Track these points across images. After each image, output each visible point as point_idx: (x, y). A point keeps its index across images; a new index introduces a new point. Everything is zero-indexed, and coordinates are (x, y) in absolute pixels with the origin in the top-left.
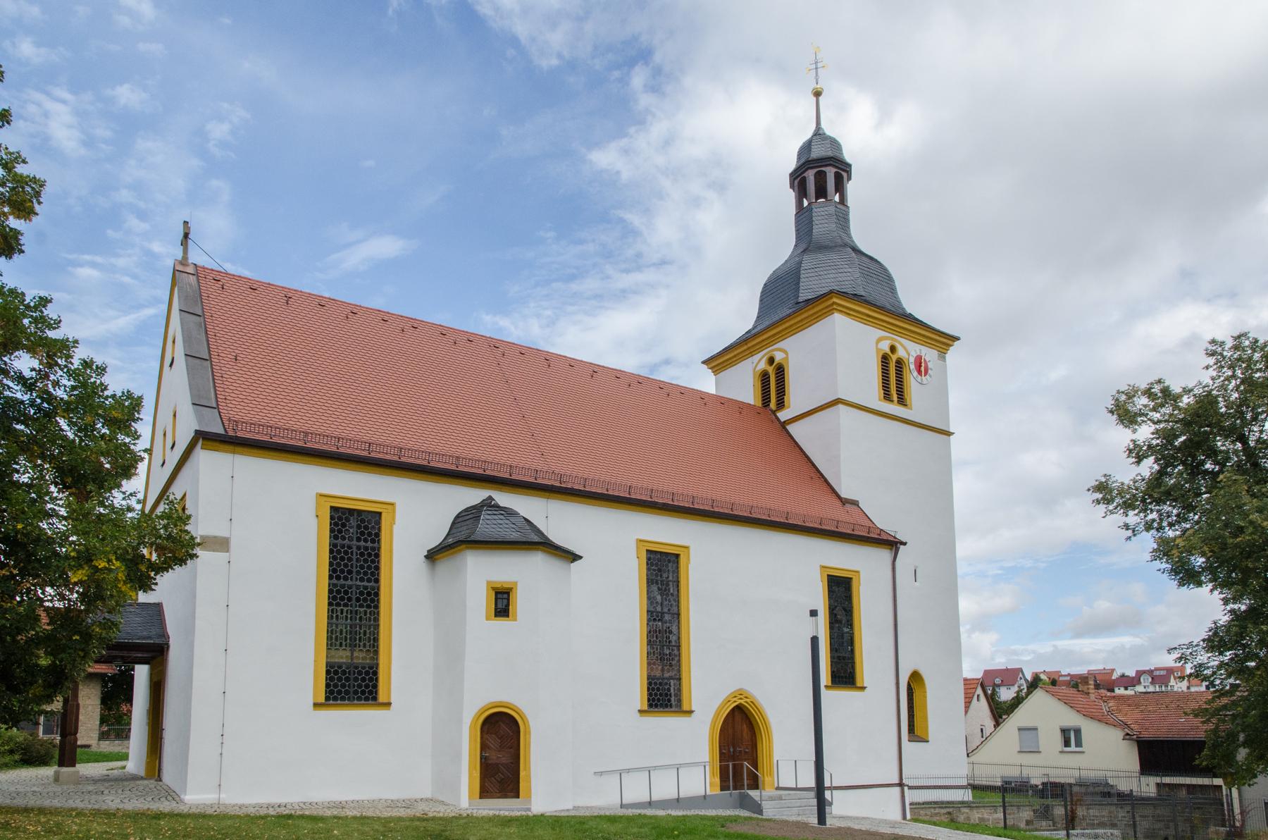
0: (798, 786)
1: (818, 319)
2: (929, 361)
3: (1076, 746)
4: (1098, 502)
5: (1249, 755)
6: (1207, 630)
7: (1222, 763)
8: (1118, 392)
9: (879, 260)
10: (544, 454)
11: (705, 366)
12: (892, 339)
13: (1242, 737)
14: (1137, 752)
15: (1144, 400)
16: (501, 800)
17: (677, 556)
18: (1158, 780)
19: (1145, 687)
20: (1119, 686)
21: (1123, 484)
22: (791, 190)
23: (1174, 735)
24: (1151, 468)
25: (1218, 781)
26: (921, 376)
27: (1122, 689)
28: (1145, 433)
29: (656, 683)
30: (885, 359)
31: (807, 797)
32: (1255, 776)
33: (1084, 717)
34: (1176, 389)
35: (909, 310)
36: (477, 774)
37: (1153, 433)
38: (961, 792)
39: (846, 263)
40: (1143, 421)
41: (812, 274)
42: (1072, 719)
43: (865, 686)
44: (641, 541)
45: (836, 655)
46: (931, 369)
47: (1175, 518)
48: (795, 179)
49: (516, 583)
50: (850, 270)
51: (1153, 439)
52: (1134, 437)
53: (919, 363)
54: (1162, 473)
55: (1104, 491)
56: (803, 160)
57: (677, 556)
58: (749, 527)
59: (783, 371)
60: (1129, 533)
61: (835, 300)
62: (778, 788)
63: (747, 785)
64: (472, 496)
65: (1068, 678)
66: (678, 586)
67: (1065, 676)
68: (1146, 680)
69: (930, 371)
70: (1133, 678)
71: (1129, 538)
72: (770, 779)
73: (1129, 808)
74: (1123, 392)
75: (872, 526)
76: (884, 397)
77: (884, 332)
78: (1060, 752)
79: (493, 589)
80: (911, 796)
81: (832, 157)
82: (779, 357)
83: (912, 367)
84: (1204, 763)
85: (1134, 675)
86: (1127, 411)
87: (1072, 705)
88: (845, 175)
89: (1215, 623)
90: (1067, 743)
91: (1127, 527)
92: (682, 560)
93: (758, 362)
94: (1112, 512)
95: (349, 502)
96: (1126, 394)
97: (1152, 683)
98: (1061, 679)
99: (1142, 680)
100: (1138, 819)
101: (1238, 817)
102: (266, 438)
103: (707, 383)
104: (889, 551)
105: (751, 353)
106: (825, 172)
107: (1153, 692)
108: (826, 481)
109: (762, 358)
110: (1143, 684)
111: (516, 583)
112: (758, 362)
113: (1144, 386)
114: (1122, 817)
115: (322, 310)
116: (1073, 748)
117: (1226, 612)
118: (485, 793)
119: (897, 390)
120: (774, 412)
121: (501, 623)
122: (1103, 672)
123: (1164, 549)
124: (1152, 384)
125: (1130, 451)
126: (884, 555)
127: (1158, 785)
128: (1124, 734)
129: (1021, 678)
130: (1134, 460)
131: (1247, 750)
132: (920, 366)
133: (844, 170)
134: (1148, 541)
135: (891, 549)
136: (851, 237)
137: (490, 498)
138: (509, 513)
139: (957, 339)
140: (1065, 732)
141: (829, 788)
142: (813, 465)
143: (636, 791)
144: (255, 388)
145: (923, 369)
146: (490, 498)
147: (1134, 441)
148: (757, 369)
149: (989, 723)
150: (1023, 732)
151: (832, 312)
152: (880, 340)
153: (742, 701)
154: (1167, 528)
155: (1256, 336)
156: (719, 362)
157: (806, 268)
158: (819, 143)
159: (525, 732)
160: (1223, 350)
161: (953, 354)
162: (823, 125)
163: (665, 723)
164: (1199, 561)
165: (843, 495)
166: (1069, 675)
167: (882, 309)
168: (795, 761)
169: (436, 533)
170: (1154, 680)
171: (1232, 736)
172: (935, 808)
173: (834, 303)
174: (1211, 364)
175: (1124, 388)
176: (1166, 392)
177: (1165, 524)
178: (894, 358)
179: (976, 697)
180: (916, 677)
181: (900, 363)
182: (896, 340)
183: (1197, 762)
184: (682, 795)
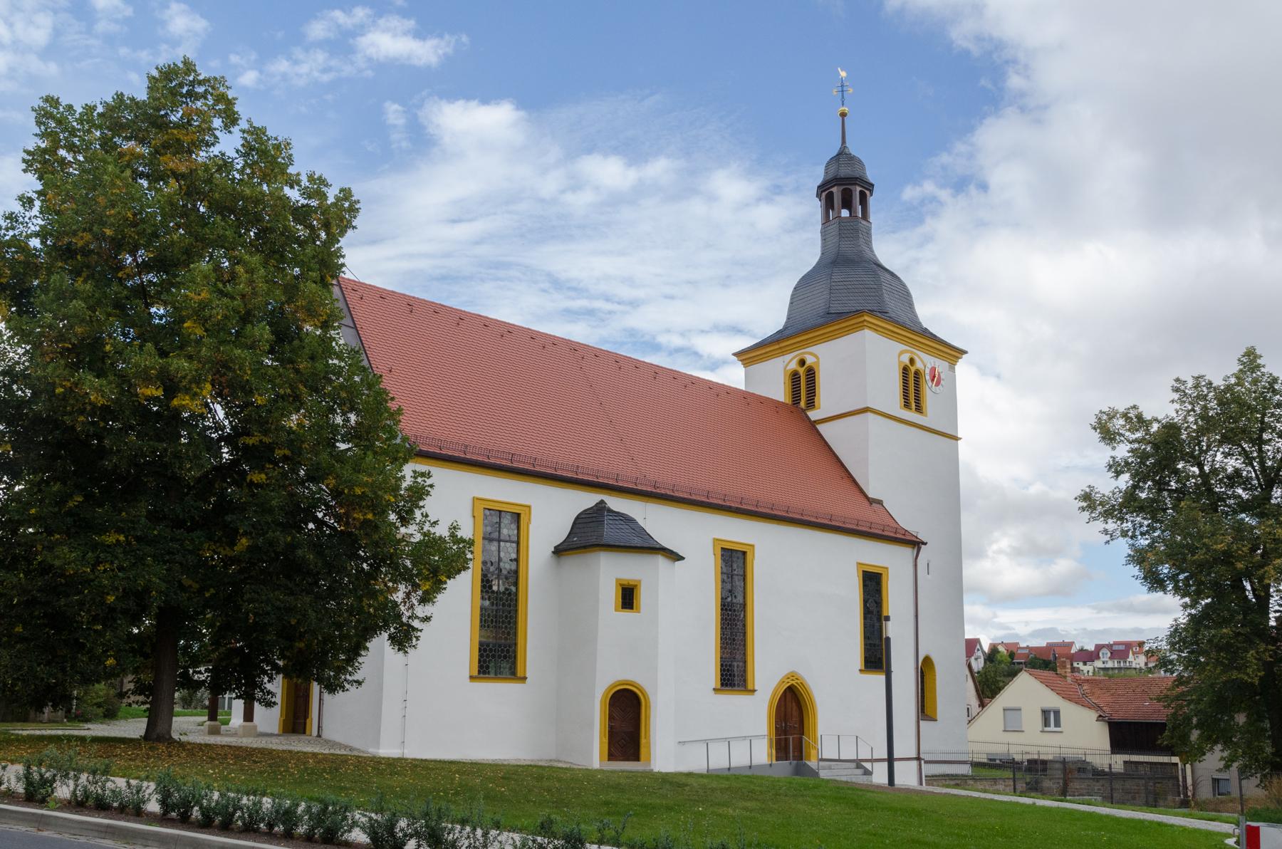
0: (886, 757)
3: (1056, 726)
4: (1083, 509)
5: (1200, 736)
6: (1169, 626)
7: (1179, 742)
8: (1101, 412)
13: (1195, 720)
15: (1122, 422)
16: (627, 762)
17: (744, 553)
18: (1127, 757)
21: (1104, 496)
24: (1127, 482)
25: (1175, 759)
27: (1081, 664)
28: (1122, 451)
30: (905, 370)
32: (1204, 754)
35: (925, 325)
36: (606, 740)
37: (1129, 452)
40: (1122, 441)
41: (842, 287)
44: (718, 540)
45: (868, 642)
47: (1146, 529)
48: (822, 192)
49: (640, 581)
51: (1129, 457)
52: (1113, 453)
54: (1135, 487)
55: (1089, 501)
56: (830, 176)
57: (744, 553)
59: (814, 373)
60: (1108, 538)
61: (866, 318)
63: (793, 756)
64: (588, 500)
65: (1027, 651)
67: (1024, 648)
70: (1092, 652)
71: (1107, 542)
74: (1104, 413)
75: (898, 529)
79: (621, 585)
80: (928, 770)
82: (810, 360)
83: (928, 377)
84: (1165, 743)
85: (1093, 649)
86: (1108, 431)
88: (867, 192)
89: (1176, 620)
90: (1046, 723)
91: (1106, 532)
94: (1095, 519)
96: (1107, 415)
98: (1019, 652)
101: (1190, 788)
103: (735, 377)
105: (783, 352)
106: (851, 191)
107: (1112, 669)
109: (792, 360)
110: (1102, 659)
111: (640, 581)
113: (1122, 410)
114: (1099, 789)
116: (1052, 728)
118: (612, 757)
120: (803, 411)
121: (627, 614)
123: (1139, 557)
124: (1129, 409)
125: (1111, 467)
126: (906, 553)
127: (1125, 762)
128: (1097, 715)
129: (978, 650)
130: (1113, 474)
131: (1198, 732)
132: (934, 377)
134: (1122, 547)
135: (914, 548)
136: (873, 251)
137: (602, 502)
138: (628, 520)
139: (965, 352)
140: (1045, 713)
142: (842, 465)
143: (719, 760)
146: (602, 502)
147: (1113, 458)
148: (788, 368)
149: (974, 702)
152: (901, 353)
154: (1140, 537)
155: (1211, 379)
156: (748, 357)
160: (1186, 388)
161: (962, 367)
163: (734, 701)
164: (1165, 569)
166: (1028, 647)
169: (560, 534)
171: (1188, 719)
174: (1176, 399)
175: (1106, 409)
176: (1140, 417)
177: (1138, 533)
178: (913, 369)
180: (927, 660)
181: (917, 374)
183: (1159, 742)
184: (754, 763)
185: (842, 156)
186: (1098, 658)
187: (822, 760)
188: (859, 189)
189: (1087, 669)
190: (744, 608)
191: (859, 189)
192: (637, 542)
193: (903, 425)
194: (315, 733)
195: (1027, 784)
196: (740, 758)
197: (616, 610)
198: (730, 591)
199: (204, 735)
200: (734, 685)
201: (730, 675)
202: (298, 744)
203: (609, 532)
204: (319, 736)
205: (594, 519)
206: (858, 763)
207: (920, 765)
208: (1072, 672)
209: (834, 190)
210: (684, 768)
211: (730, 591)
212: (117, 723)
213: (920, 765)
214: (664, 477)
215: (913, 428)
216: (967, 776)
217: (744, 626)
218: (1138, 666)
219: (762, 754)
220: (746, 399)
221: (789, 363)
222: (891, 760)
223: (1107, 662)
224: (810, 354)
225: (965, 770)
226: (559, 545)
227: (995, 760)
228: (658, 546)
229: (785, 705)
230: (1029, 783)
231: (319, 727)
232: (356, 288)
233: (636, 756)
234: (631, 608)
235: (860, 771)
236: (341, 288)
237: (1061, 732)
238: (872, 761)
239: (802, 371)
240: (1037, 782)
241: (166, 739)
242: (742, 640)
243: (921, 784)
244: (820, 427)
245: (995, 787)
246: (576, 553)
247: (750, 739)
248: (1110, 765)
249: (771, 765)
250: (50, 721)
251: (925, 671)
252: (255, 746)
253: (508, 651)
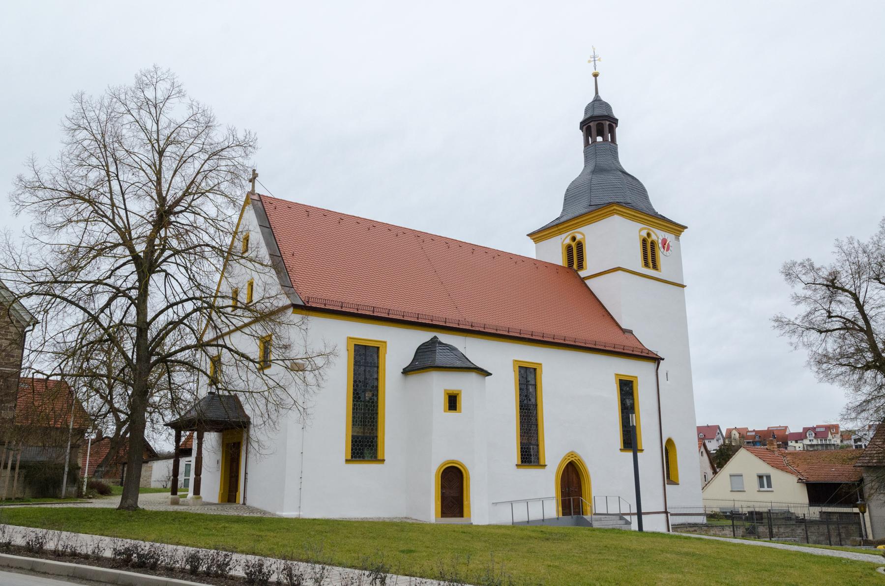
12: (648, 229)
14: (806, 489)
17: (535, 369)
19: (810, 441)
20: (791, 440)
22: (581, 131)
23: (828, 479)
25: (856, 510)
27: (794, 442)
29: (525, 448)
30: (644, 241)
34: (817, 266)
36: (439, 503)
38: (702, 517)
42: (764, 468)
44: (516, 361)
49: (460, 391)
50: (621, 186)
53: (664, 242)
60: (792, 348)
64: (425, 336)
65: (754, 433)
66: (536, 388)
68: (811, 436)
69: (670, 248)
73: (804, 527)
75: (643, 349)
79: (448, 394)
80: (673, 520)
81: (606, 116)
82: (579, 237)
83: (660, 245)
88: (614, 125)
90: (762, 486)
91: (791, 344)
92: (538, 371)
93: (564, 239)
97: (815, 437)
98: (748, 434)
99: (808, 435)
100: (809, 534)
103: (529, 250)
104: (653, 364)
105: (560, 233)
107: (817, 445)
108: (612, 317)
109: (567, 237)
110: (809, 438)
111: (460, 391)
112: (564, 239)
113: (799, 262)
116: (766, 488)
120: (576, 271)
121: (452, 414)
122: (779, 428)
126: (650, 366)
129: (718, 434)
132: (665, 244)
133: (614, 123)
135: (655, 363)
137: (435, 337)
139: (686, 228)
140: (760, 477)
141: (634, 514)
143: (520, 515)
145: (666, 246)
146: (435, 337)
148: (564, 243)
149: (710, 471)
150: (733, 478)
152: (641, 230)
153: (573, 459)
156: (539, 235)
159: (467, 478)
161: (684, 235)
162: (600, 94)
163: (531, 473)
165: (623, 327)
166: (754, 431)
167: (641, 212)
169: (407, 358)
170: (817, 435)
178: (650, 240)
180: (670, 442)
181: (653, 243)
184: (530, 519)
185: (597, 100)
186: (806, 438)
187: (595, 514)
188: (608, 123)
189: (798, 446)
190: (536, 407)
191: (608, 123)
192: (458, 364)
193: (675, 287)
194: (241, 502)
195: (747, 529)
196: (536, 514)
197: (445, 411)
198: (526, 396)
199: (169, 505)
200: (531, 462)
201: (528, 455)
202: (231, 511)
203: (441, 358)
204: (244, 504)
205: (429, 349)
206: (621, 516)
207: (667, 517)
208: (779, 448)
209: (591, 124)
210: (494, 521)
211: (526, 396)
212: (109, 497)
213: (667, 517)
214: (491, 322)
215: (625, 273)
216: (702, 524)
217: (537, 420)
218: (835, 443)
219: (552, 510)
220: (536, 264)
221: (565, 239)
222: (639, 514)
223: (812, 440)
224: (578, 232)
225: (702, 520)
226: (405, 368)
227: (726, 512)
228: (472, 366)
229: (568, 475)
230: (748, 529)
231: (244, 498)
232: (272, 202)
233: (460, 514)
234: (455, 409)
235: (622, 522)
236: (262, 202)
237: (772, 491)
238: (630, 514)
239: (574, 244)
240: (754, 528)
241: (135, 508)
242: (535, 430)
243: (669, 531)
244: (588, 282)
245: (723, 532)
246: (416, 373)
247: (543, 500)
248: (804, 515)
249: (558, 518)
250: (66, 498)
251: (668, 450)
252: (199, 512)
253: (372, 442)
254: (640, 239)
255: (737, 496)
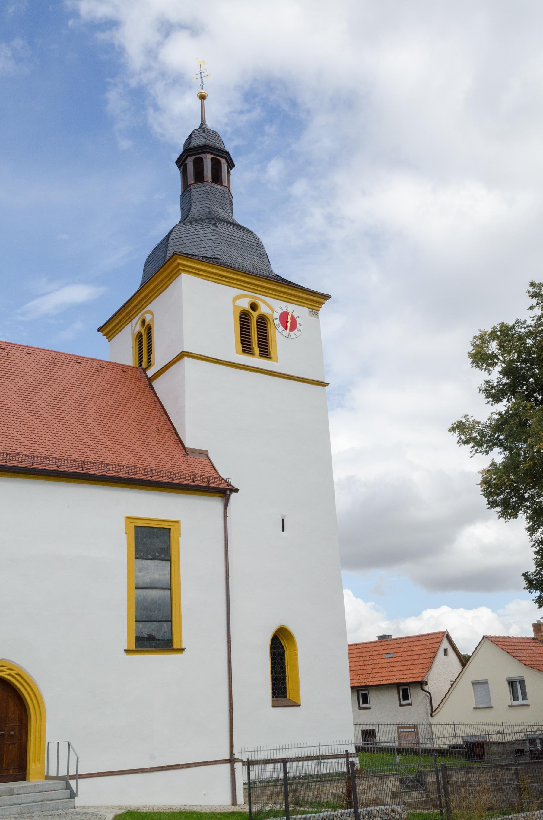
1: (171, 280)
2: (298, 317)
9: (249, 228)
10: (189, 461)
11: (100, 334)
26: (286, 329)
31: (52, 789)
33: (525, 667)
39: (209, 231)
43: (183, 647)
46: (301, 325)
52: (488, 378)
58: (161, 491)
61: (179, 261)
62: (48, 778)
72: (38, 766)
76: (260, 353)
77: (267, 301)
78: (509, 706)
83: (277, 322)
87: (515, 655)
90: (515, 698)
95: (152, 522)
102: (54, 468)
109: (137, 323)
115: (29, 357)
117: (533, 543)
119: (259, 344)
140: (512, 684)
144: (15, 427)
147: (487, 382)
148: (135, 332)
151: (179, 273)
157: (174, 238)
158: (198, 135)
165: (188, 444)
168: (58, 743)
172: (276, 785)
173: (179, 264)
179: (441, 652)
181: (263, 322)
182: (258, 298)
191: (209, 156)
254: (235, 310)
255: (485, 717)
